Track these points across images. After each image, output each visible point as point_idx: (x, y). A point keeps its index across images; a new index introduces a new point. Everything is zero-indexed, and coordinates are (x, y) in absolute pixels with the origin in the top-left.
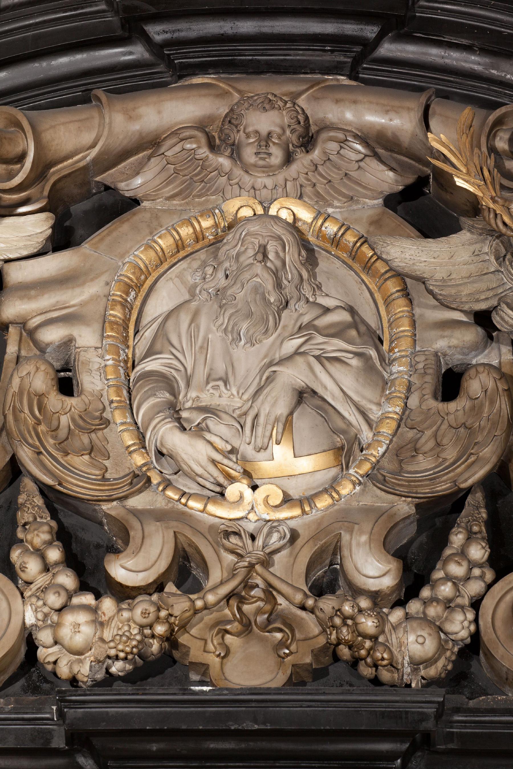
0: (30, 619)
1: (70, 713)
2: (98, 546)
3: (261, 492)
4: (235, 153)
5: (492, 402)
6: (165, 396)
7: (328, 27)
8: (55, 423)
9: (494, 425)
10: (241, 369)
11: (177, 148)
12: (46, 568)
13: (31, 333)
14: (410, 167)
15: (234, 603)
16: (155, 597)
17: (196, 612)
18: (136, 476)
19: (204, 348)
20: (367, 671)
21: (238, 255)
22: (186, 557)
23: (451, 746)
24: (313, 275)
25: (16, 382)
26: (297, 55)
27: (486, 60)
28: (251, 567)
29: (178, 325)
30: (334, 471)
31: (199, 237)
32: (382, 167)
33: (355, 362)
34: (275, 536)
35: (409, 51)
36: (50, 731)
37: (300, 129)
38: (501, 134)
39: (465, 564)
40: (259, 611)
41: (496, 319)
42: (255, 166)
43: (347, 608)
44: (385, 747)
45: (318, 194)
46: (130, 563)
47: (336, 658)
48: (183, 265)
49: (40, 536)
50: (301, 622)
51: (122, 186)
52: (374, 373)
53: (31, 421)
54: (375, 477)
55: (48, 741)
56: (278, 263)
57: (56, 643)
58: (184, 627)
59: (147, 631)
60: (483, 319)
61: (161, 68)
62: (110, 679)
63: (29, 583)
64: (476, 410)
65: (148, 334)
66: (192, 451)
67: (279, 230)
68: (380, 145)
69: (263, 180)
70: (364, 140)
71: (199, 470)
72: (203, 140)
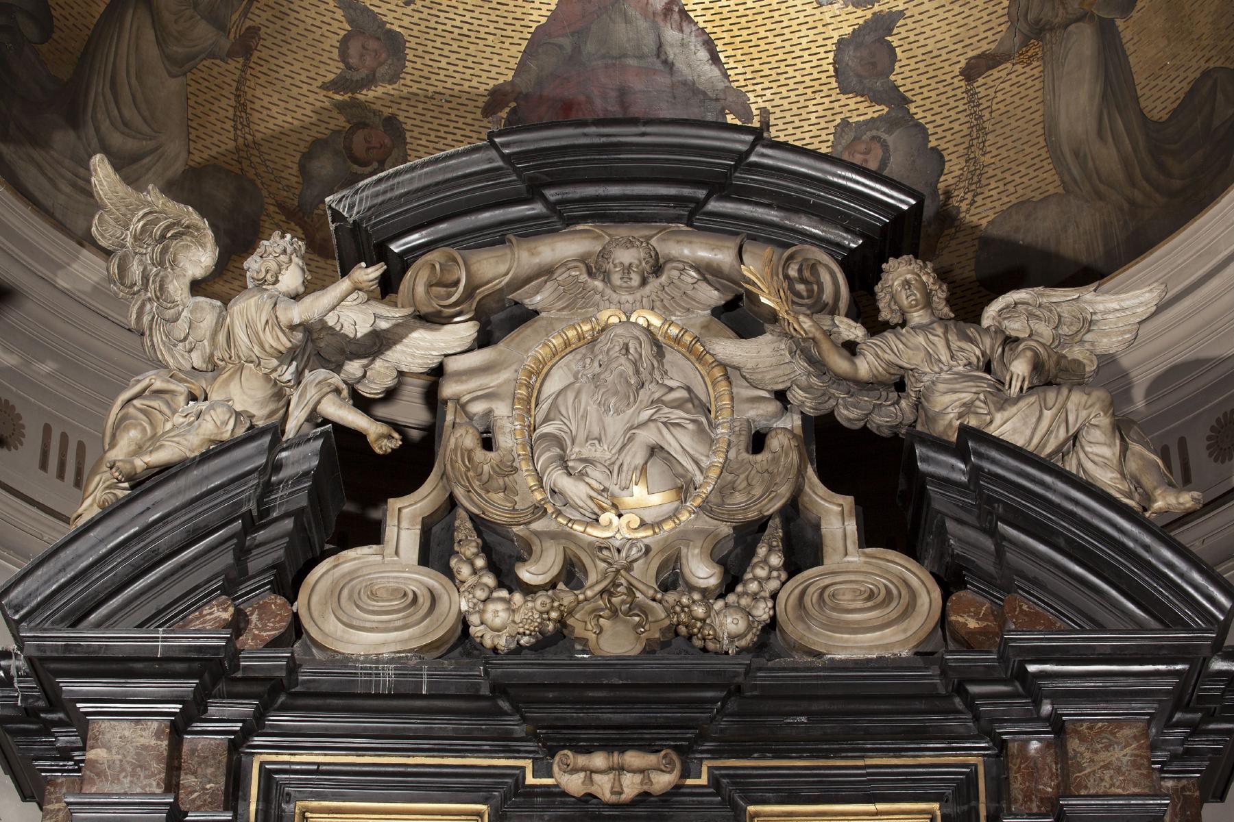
0: (464, 607)
1: (493, 672)
2: (511, 556)
3: (624, 519)
4: (606, 277)
5: (787, 455)
6: (556, 451)
7: (672, 191)
8: (479, 470)
9: (788, 471)
10: (611, 430)
11: (565, 275)
12: (475, 572)
13: (463, 407)
14: (730, 288)
15: (605, 596)
16: (550, 592)
17: (579, 603)
18: (536, 507)
19: (585, 416)
20: (698, 643)
21: (608, 350)
22: (572, 565)
23: (755, 693)
24: (661, 364)
25: (453, 441)
26: (651, 210)
27: (782, 214)
28: (618, 571)
29: (565, 400)
30: (676, 504)
31: (580, 337)
32: (710, 288)
33: (691, 426)
34: (634, 550)
35: (729, 207)
36: (479, 684)
37: (652, 261)
38: (792, 266)
39: (767, 568)
40: (623, 602)
41: (789, 396)
42: (621, 287)
43: (685, 600)
44: (710, 694)
45: (665, 307)
46: (532, 569)
47: (677, 634)
48: (570, 357)
49: (470, 550)
50: (652, 609)
51: (527, 301)
52: (704, 434)
53: (463, 469)
54: (705, 508)
55: (478, 690)
56: (637, 356)
57: (482, 623)
58: (571, 613)
59: (545, 616)
60: (781, 396)
61: (555, 219)
62: (520, 648)
63: (463, 582)
64: (775, 460)
65: (545, 407)
66: (576, 490)
67: (637, 333)
68: (708, 272)
69: (626, 297)
70: (697, 269)
71: (581, 504)
72: (584, 269)
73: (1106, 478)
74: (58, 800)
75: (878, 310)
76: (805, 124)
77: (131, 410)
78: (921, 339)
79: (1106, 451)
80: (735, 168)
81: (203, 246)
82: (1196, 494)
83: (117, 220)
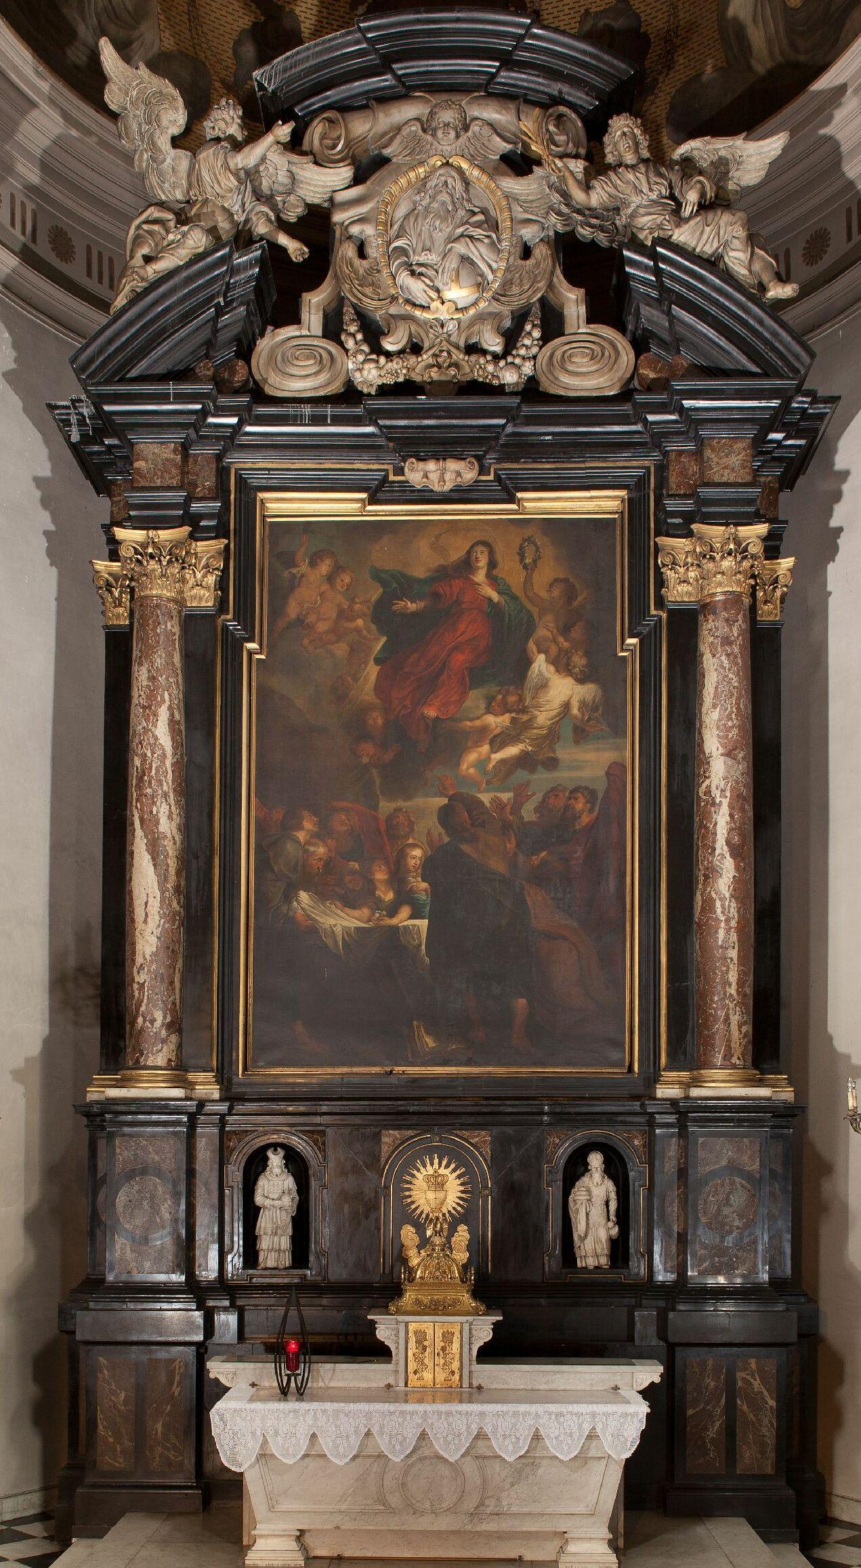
12: (356, 343)
33: (486, 241)
49: (353, 328)
64: (538, 265)
65: (396, 227)
73: (741, 271)
74: (120, 495)
75: (605, 156)
76: (561, 14)
77: (141, 232)
78: (631, 176)
79: (740, 255)
80: (515, 47)
81: (177, 109)
82: (795, 286)
83: (120, 89)
